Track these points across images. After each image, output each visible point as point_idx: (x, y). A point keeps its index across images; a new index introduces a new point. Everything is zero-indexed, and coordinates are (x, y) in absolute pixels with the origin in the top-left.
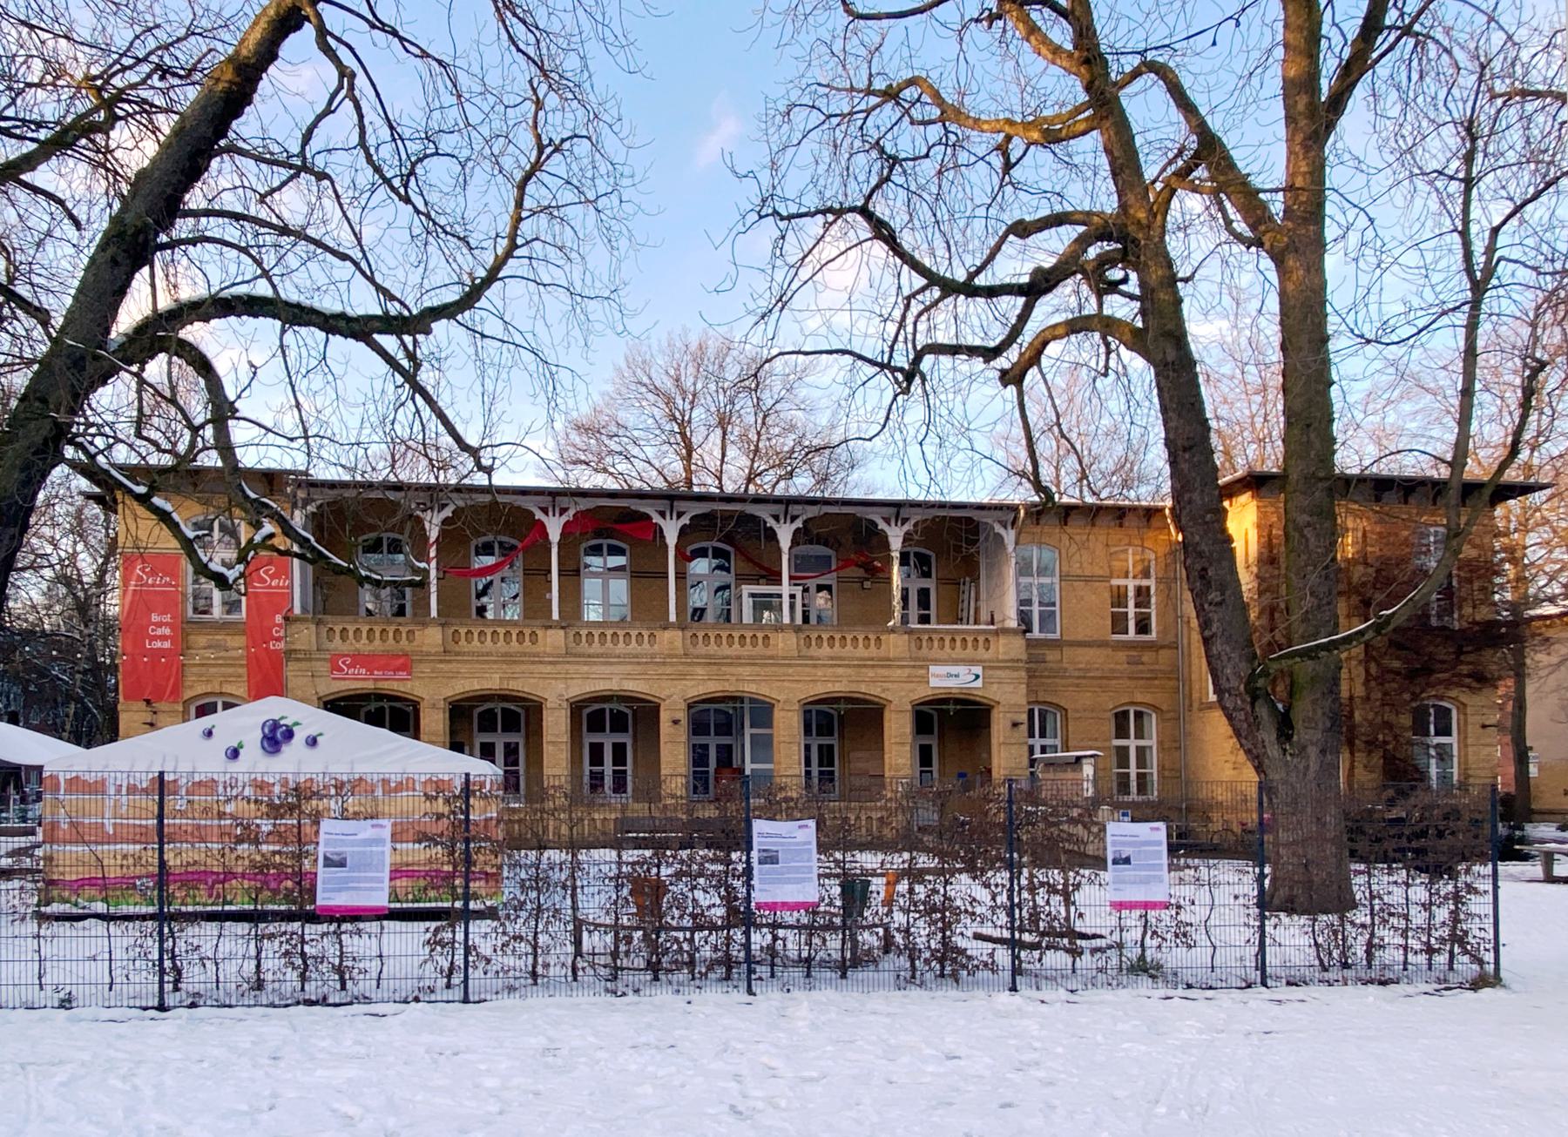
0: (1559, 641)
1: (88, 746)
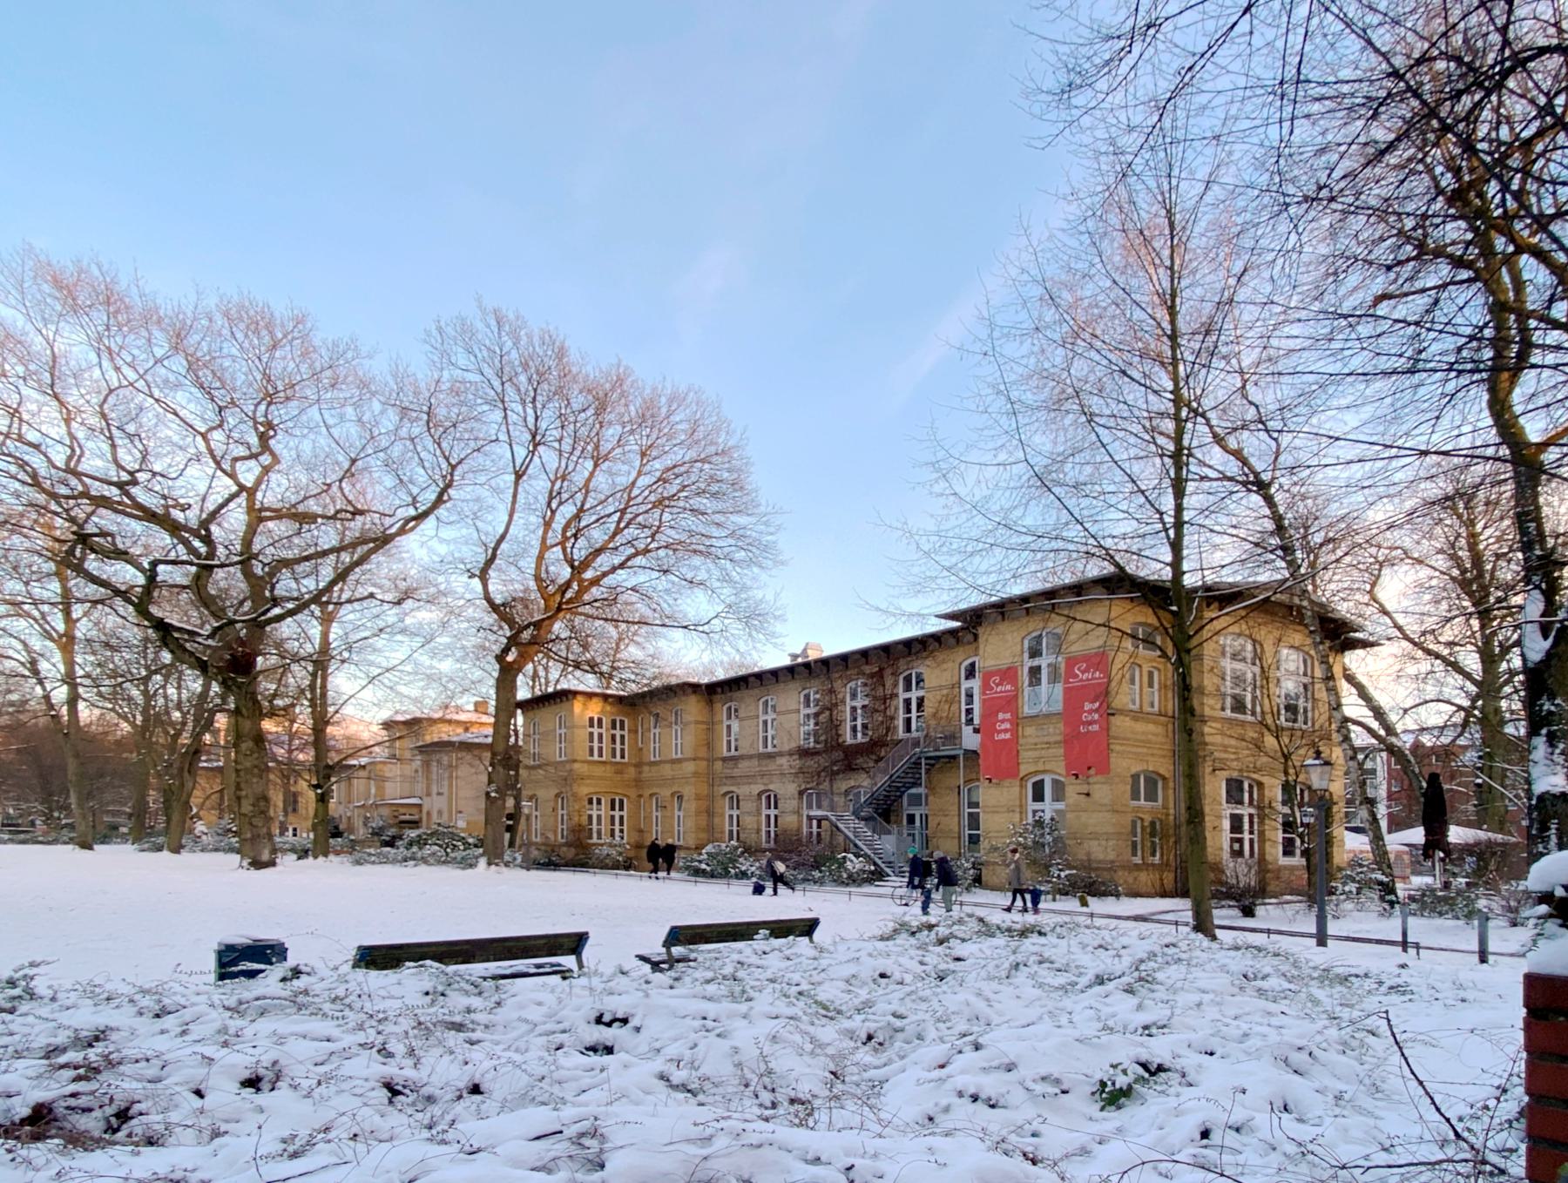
0: (564, 342)
1: (86, 846)
